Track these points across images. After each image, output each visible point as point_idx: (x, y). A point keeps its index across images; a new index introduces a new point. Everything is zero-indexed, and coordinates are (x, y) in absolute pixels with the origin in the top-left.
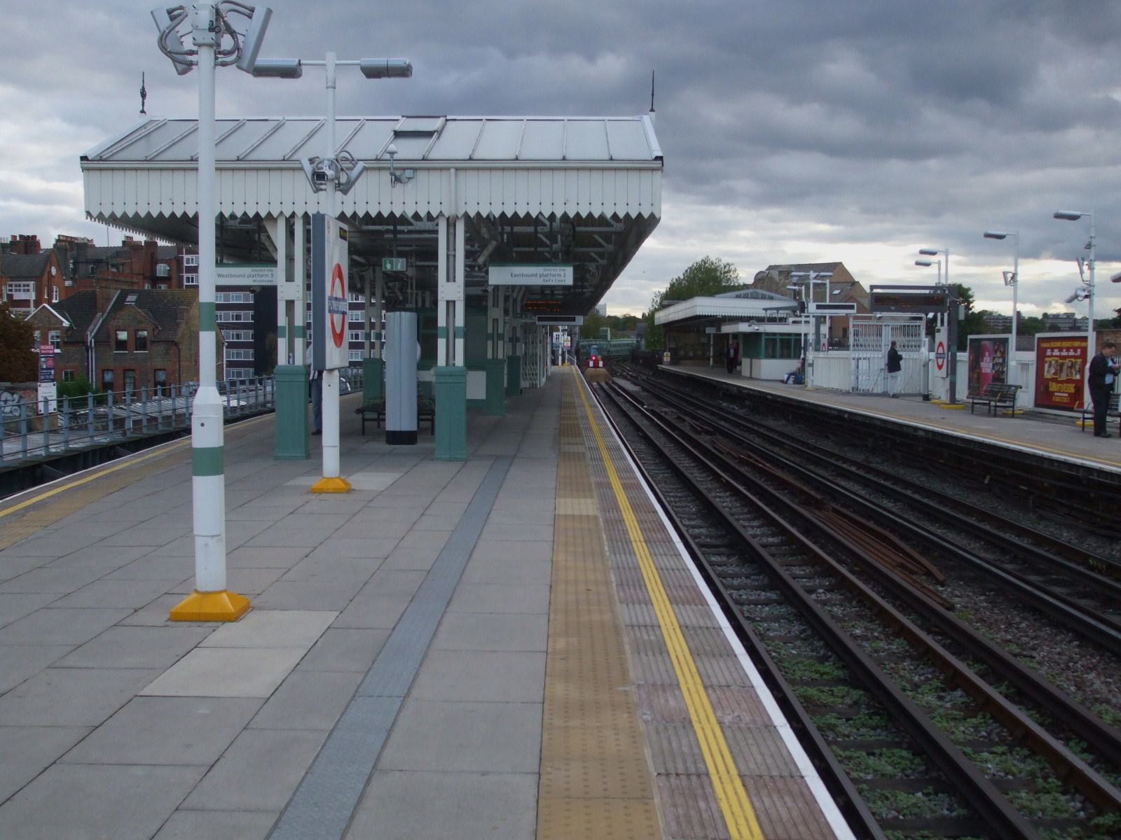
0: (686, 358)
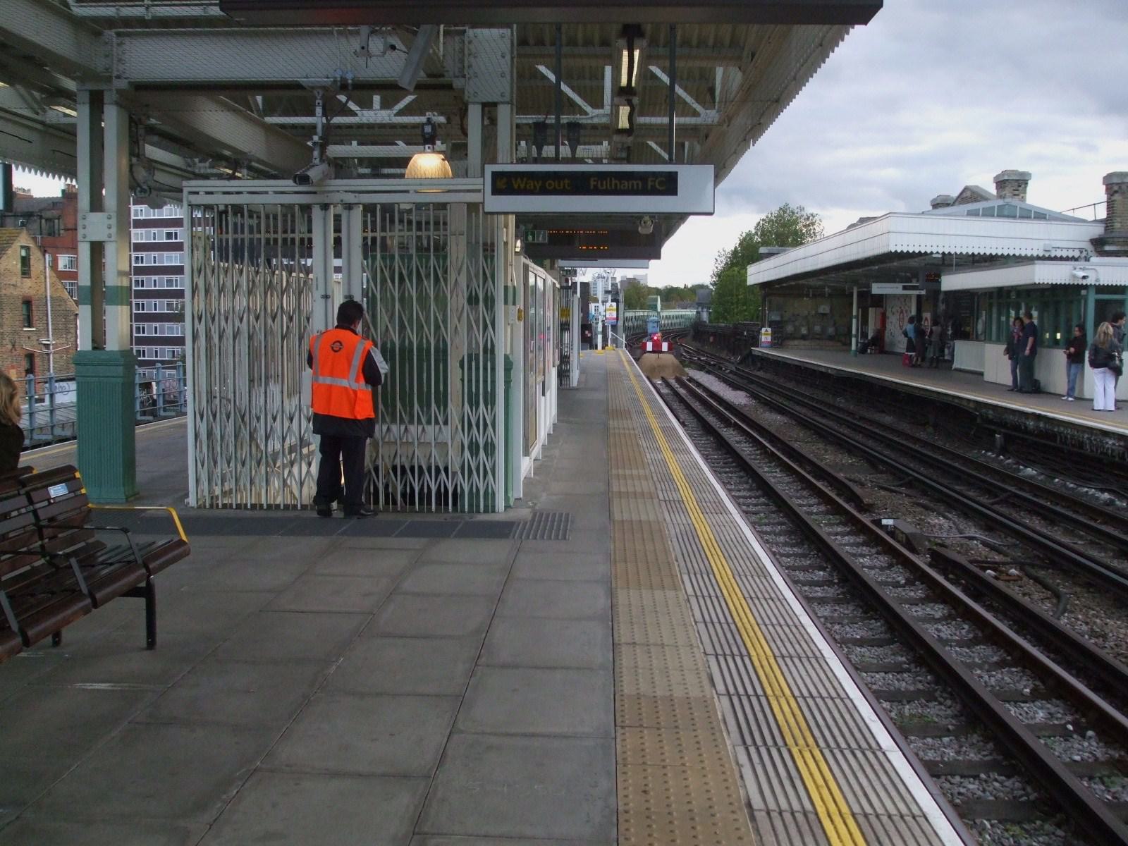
0: (792, 337)
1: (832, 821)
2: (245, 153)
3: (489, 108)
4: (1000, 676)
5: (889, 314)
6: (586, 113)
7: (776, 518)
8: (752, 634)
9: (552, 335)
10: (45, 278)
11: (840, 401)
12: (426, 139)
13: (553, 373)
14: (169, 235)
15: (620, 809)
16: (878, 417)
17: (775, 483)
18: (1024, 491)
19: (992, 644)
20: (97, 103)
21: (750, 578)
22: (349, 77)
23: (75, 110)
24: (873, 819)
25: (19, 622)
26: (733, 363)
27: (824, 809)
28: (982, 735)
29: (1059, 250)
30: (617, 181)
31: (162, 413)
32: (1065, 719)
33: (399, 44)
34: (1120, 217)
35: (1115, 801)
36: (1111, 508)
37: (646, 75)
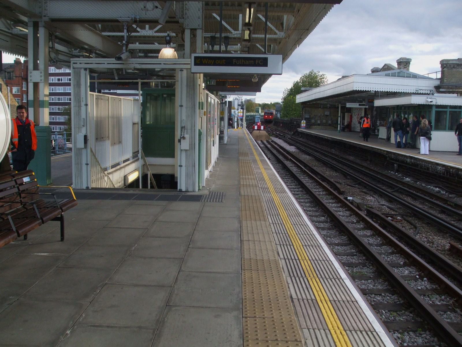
0: (314, 124)
1: (322, 302)
2: (94, 47)
3: (193, 31)
4: (391, 257)
5: (353, 115)
6: (232, 33)
7: (305, 196)
8: (294, 237)
9: (217, 121)
10: (8, 97)
11: (333, 151)
12: (167, 43)
13: (217, 137)
14: (59, 80)
15: (243, 298)
16: (348, 157)
17: (306, 183)
18: (405, 187)
19: (389, 246)
20: (36, 26)
21: (294, 217)
22: (138, 17)
23: (27, 29)
24: (337, 302)
25: (16, 228)
26: (290, 135)
27: (319, 299)
28: (383, 280)
29: (422, 91)
30: (244, 61)
31: (58, 153)
32: (416, 273)
33: (159, 6)
34: (446, 77)
35: (433, 304)
36: (439, 194)
37: (256, 18)
